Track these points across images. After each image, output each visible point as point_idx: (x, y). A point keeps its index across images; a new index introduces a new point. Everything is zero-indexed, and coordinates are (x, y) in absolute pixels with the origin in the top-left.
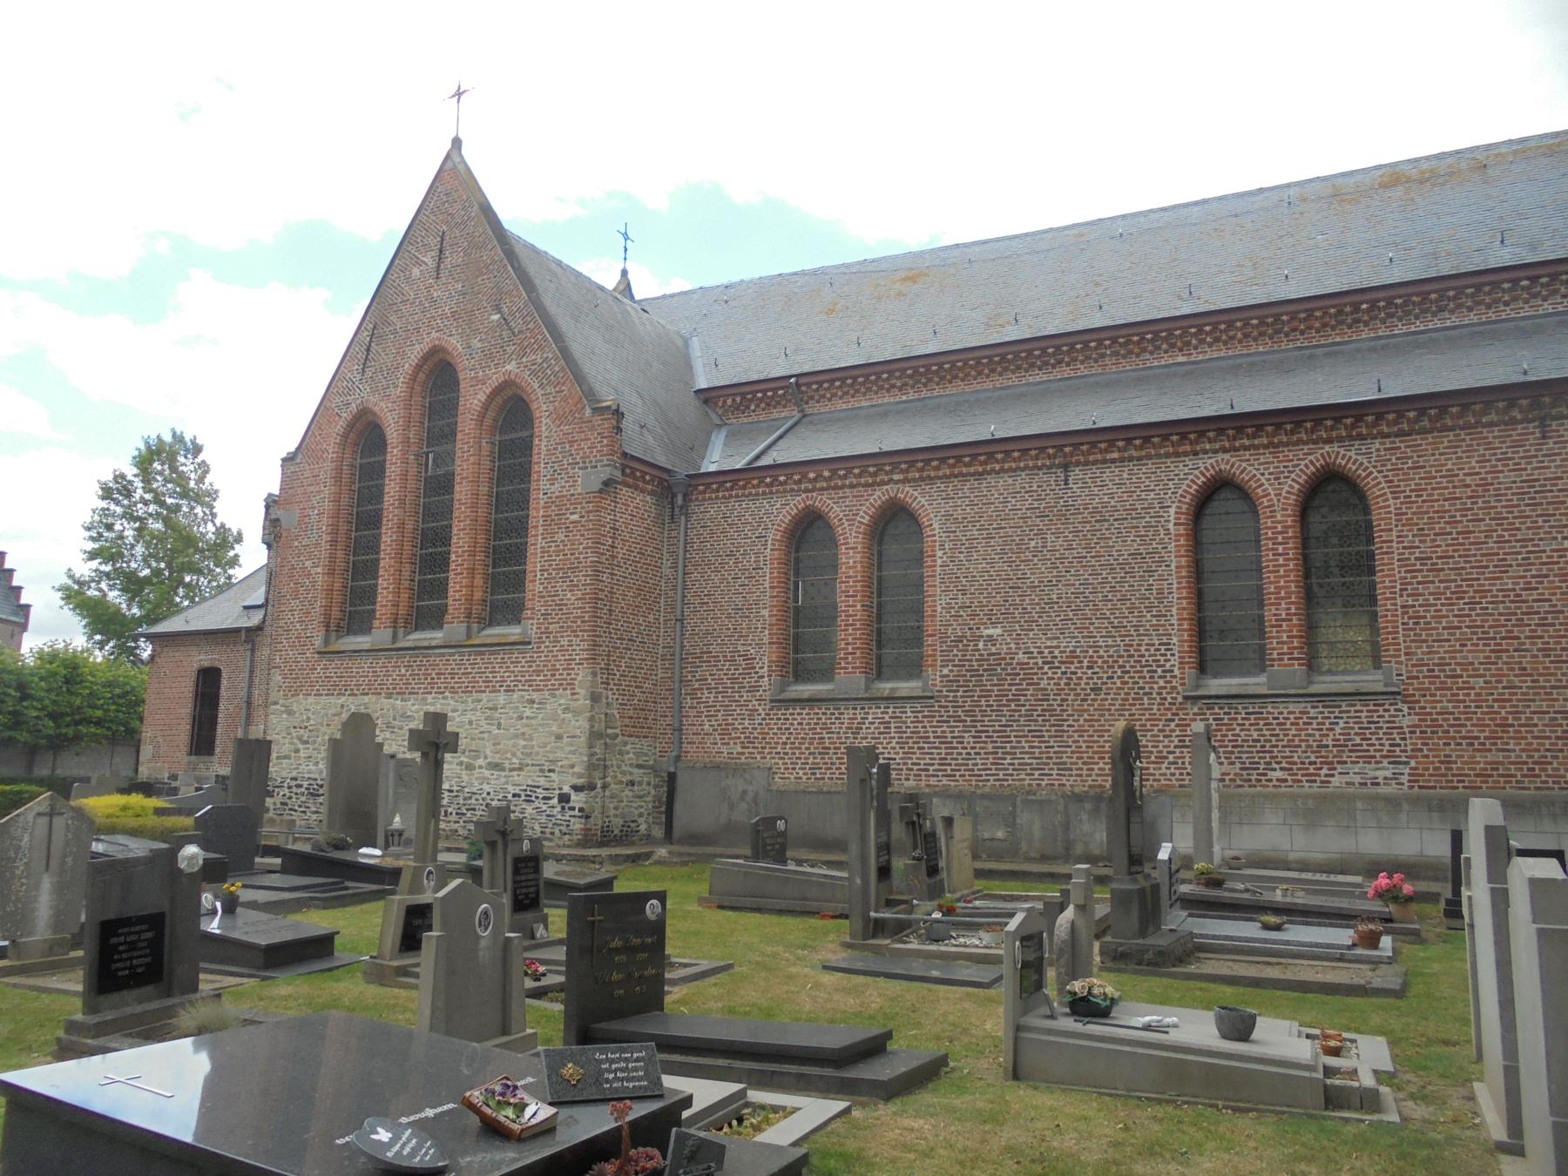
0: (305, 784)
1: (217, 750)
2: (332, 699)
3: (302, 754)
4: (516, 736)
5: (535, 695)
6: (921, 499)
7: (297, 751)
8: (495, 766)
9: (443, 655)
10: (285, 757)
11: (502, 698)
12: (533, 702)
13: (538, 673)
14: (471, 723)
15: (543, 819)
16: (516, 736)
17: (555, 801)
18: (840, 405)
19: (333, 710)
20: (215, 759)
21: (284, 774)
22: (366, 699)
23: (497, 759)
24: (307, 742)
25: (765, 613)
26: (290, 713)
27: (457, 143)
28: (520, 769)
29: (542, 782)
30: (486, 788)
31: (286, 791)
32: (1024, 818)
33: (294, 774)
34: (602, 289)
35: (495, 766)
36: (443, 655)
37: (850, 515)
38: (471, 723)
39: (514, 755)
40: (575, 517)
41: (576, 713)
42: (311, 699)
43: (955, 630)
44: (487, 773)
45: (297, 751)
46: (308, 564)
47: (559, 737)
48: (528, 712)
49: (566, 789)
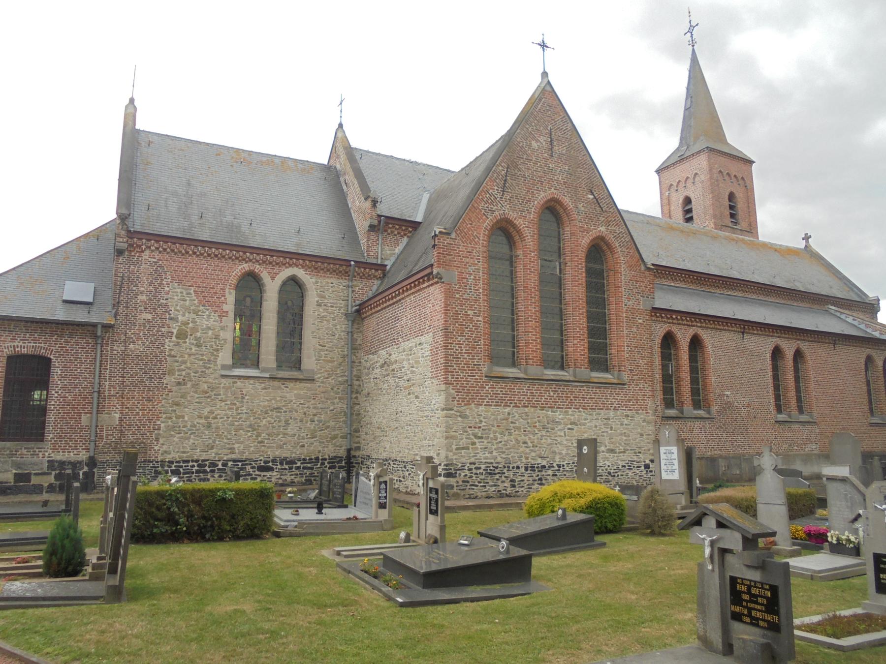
0: (483, 467)
1: (49, 437)
2: (500, 409)
3: (478, 445)
4: (621, 434)
5: (629, 413)
6: (706, 336)
7: (474, 444)
8: (612, 451)
9: (577, 386)
10: (463, 448)
11: (612, 414)
12: (628, 416)
13: (629, 401)
14: (596, 427)
15: (637, 478)
16: (621, 434)
17: (643, 468)
18: (754, 296)
19: (502, 416)
20: (48, 445)
21: (463, 460)
22: (526, 409)
23: (612, 447)
24: (481, 438)
25: (657, 376)
26: (464, 416)
27: (545, 74)
28: (624, 452)
29: (635, 458)
30: (607, 463)
31: (467, 472)
32: (744, 465)
33: (473, 460)
34: (135, 124)
35: (612, 451)
36: (577, 386)
37: (683, 336)
38: (596, 427)
39: (620, 444)
40: (640, 321)
41: (649, 423)
42: (482, 408)
43: (718, 391)
44: (607, 455)
45: (474, 444)
46: (469, 312)
47: (642, 435)
48: (626, 422)
49: (647, 462)
